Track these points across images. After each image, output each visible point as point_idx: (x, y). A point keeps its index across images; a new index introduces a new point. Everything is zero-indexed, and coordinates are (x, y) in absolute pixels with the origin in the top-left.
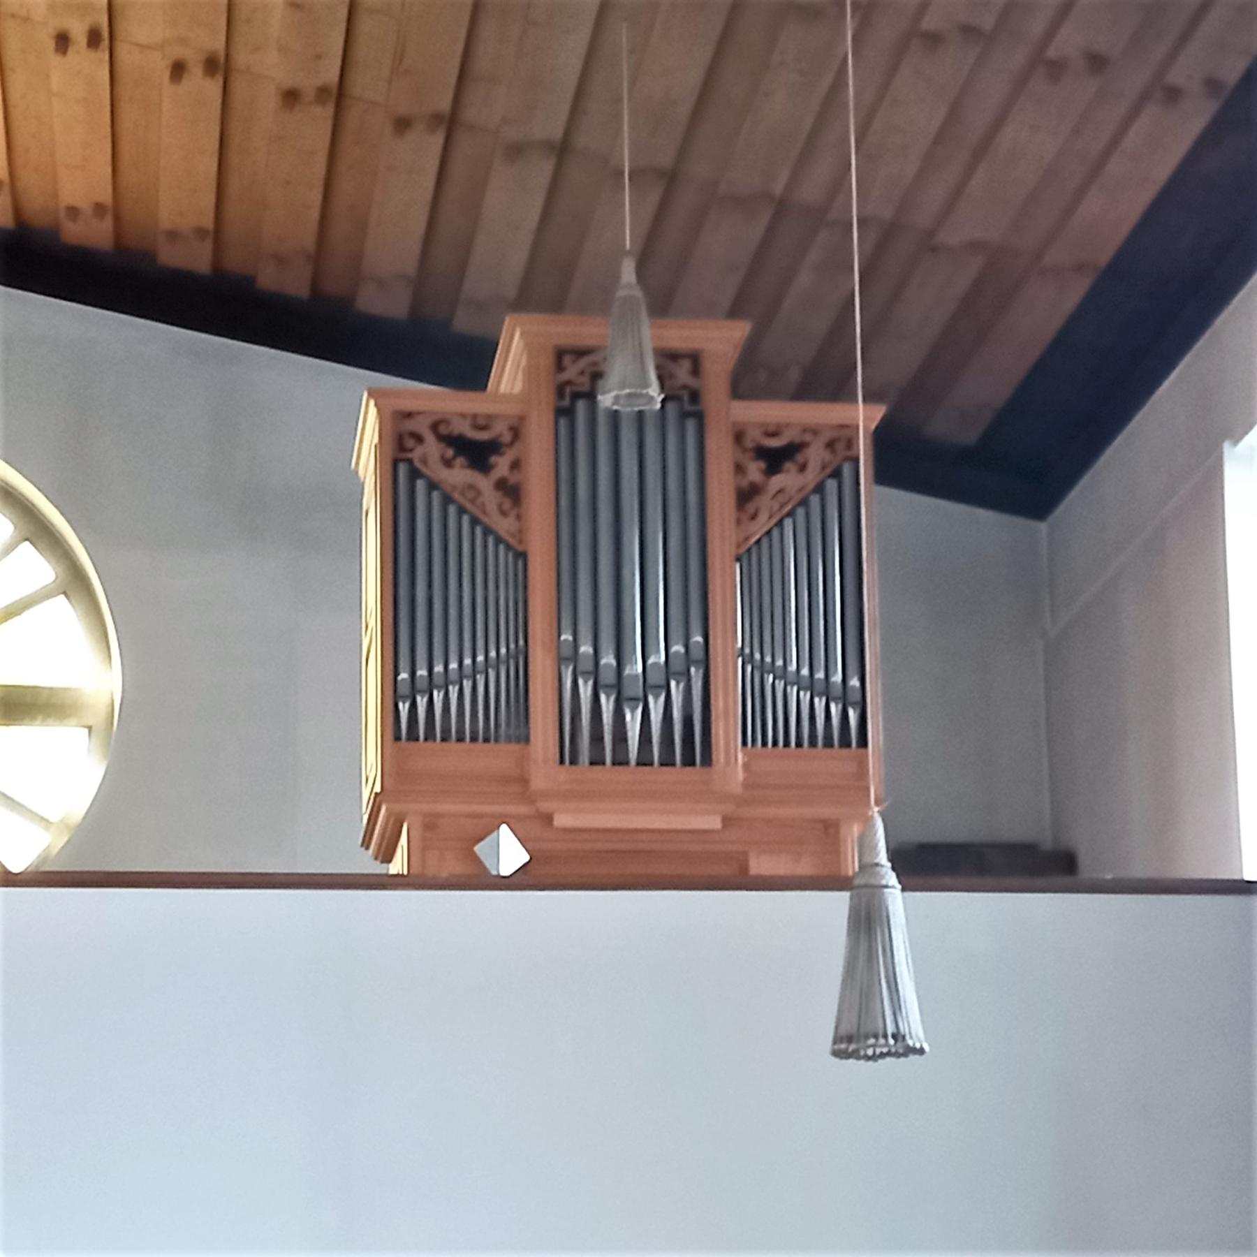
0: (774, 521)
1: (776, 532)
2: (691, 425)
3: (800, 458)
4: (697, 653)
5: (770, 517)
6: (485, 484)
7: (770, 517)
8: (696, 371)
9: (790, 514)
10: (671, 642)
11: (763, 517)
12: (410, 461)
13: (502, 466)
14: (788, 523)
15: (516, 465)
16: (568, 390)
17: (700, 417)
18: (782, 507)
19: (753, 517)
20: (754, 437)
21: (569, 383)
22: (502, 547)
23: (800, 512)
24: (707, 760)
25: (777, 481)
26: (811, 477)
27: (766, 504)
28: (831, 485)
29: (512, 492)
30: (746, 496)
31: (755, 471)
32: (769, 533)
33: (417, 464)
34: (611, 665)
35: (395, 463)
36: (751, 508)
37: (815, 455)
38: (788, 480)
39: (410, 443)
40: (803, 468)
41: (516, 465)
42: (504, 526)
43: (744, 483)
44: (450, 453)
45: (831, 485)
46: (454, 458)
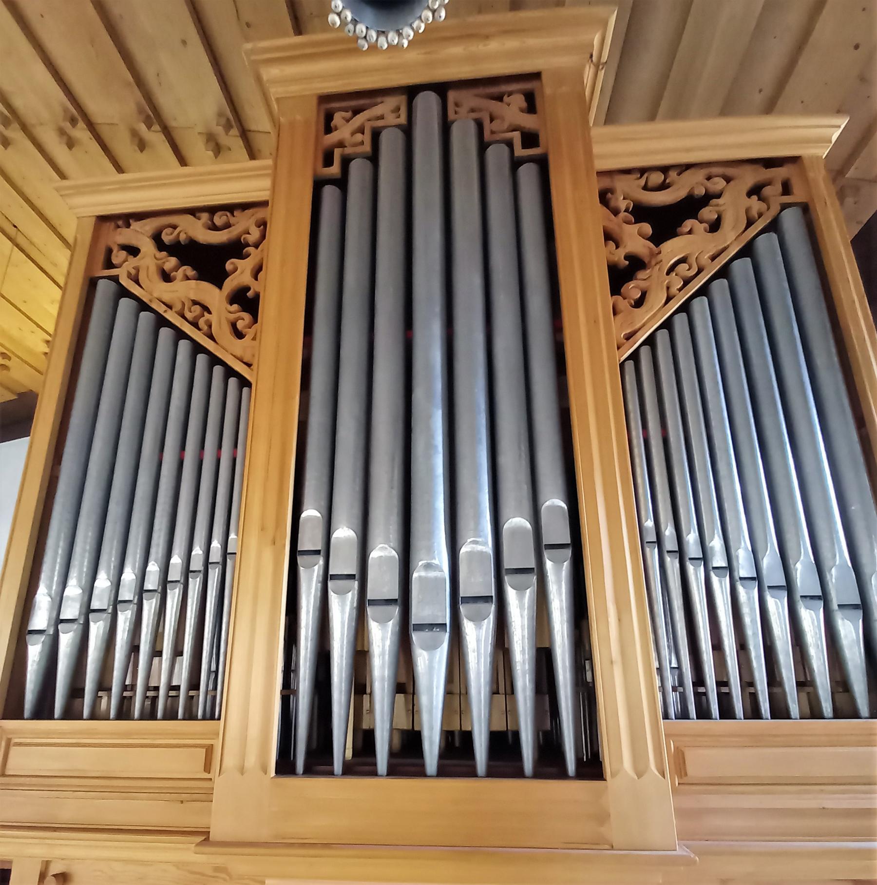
0: (675, 305)
1: (681, 321)
2: (528, 174)
3: (708, 213)
4: (557, 530)
5: (669, 299)
6: (214, 297)
7: (669, 299)
8: (531, 105)
9: (704, 291)
10: (542, 496)
11: (657, 298)
12: (115, 279)
13: (240, 272)
14: (700, 306)
15: (257, 271)
16: (337, 153)
17: (543, 164)
18: (687, 282)
19: (639, 303)
20: (628, 191)
21: (341, 144)
22: (201, 359)
23: (720, 287)
24: (592, 767)
25: (673, 249)
26: (731, 237)
27: (654, 281)
28: (742, 268)
29: (247, 301)
30: (620, 276)
31: (635, 239)
32: (668, 325)
33: (125, 282)
34: (394, 557)
35: (92, 284)
36: (632, 289)
37: (733, 205)
38: (692, 243)
39: (118, 256)
40: (715, 226)
41: (257, 271)
42: (229, 349)
43: (619, 257)
44: (173, 261)
45: (767, 245)
46: (176, 269)
